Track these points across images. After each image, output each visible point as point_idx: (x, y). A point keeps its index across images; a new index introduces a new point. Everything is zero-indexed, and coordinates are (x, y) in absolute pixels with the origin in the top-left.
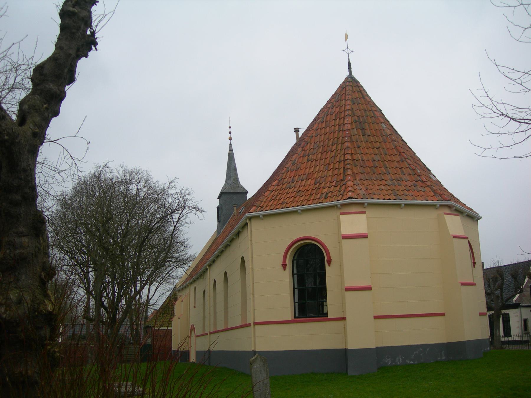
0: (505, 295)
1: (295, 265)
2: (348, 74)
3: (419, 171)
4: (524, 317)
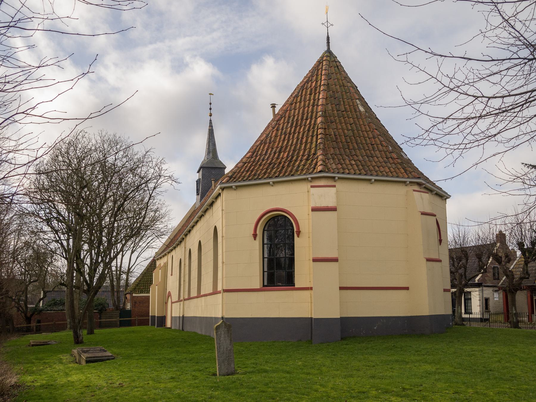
0: (469, 276)
1: (265, 237)
2: (326, 49)
3: (390, 148)
4: (485, 296)
